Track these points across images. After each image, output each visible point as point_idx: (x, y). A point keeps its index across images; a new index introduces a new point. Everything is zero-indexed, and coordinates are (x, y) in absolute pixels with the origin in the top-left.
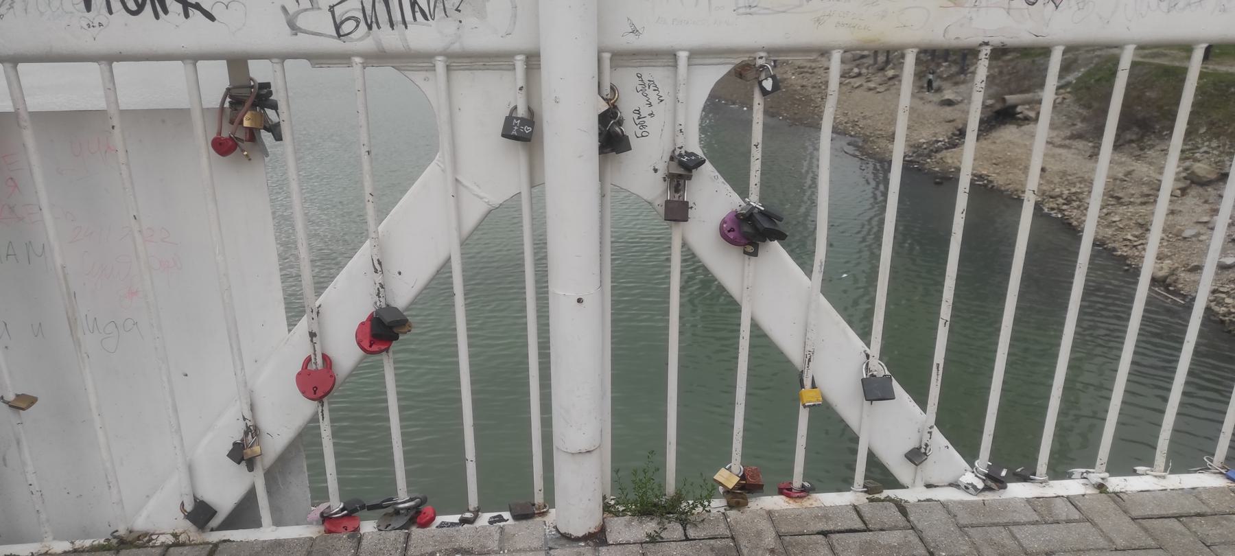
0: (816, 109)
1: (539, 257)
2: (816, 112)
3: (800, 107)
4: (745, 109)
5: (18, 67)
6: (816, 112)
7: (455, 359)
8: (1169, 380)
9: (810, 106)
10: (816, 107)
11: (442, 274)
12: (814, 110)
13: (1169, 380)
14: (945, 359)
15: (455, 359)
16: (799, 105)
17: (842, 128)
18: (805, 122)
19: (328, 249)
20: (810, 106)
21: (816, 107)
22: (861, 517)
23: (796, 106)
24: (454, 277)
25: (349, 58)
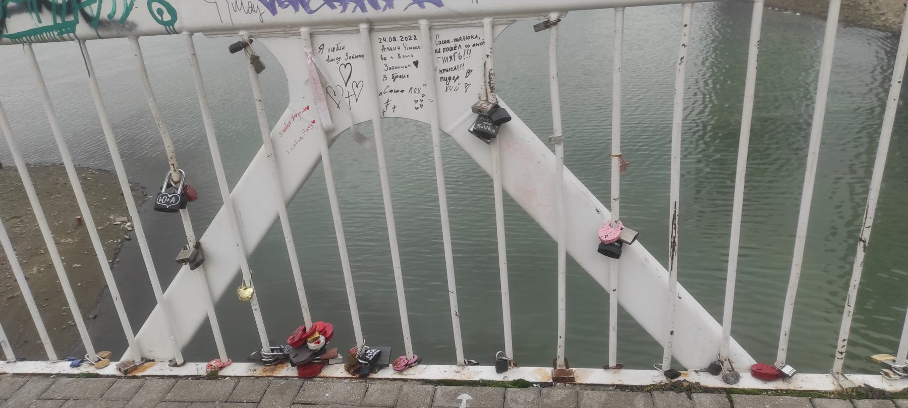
0: (866, 12)
1: (700, 150)
2: (866, 14)
3: (850, 11)
4: (798, 14)
5: (139, 40)
6: (866, 14)
7: (509, 255)
8: (727, 213)
9: (860, 10)
10: (866, 11)
11: (275, 226)
12: (865, 13)
13: (727, 213)
14: (870, 237)
15: (509, 255)
16: (848, 9)
17: (896, 28)
18: (859, 24)
19: (159, 151)
20: (860, 10)
21: (866, 11)
22: (846, 378)
23: (846, 10)
24: (613, 139)
25: (617, 365)
